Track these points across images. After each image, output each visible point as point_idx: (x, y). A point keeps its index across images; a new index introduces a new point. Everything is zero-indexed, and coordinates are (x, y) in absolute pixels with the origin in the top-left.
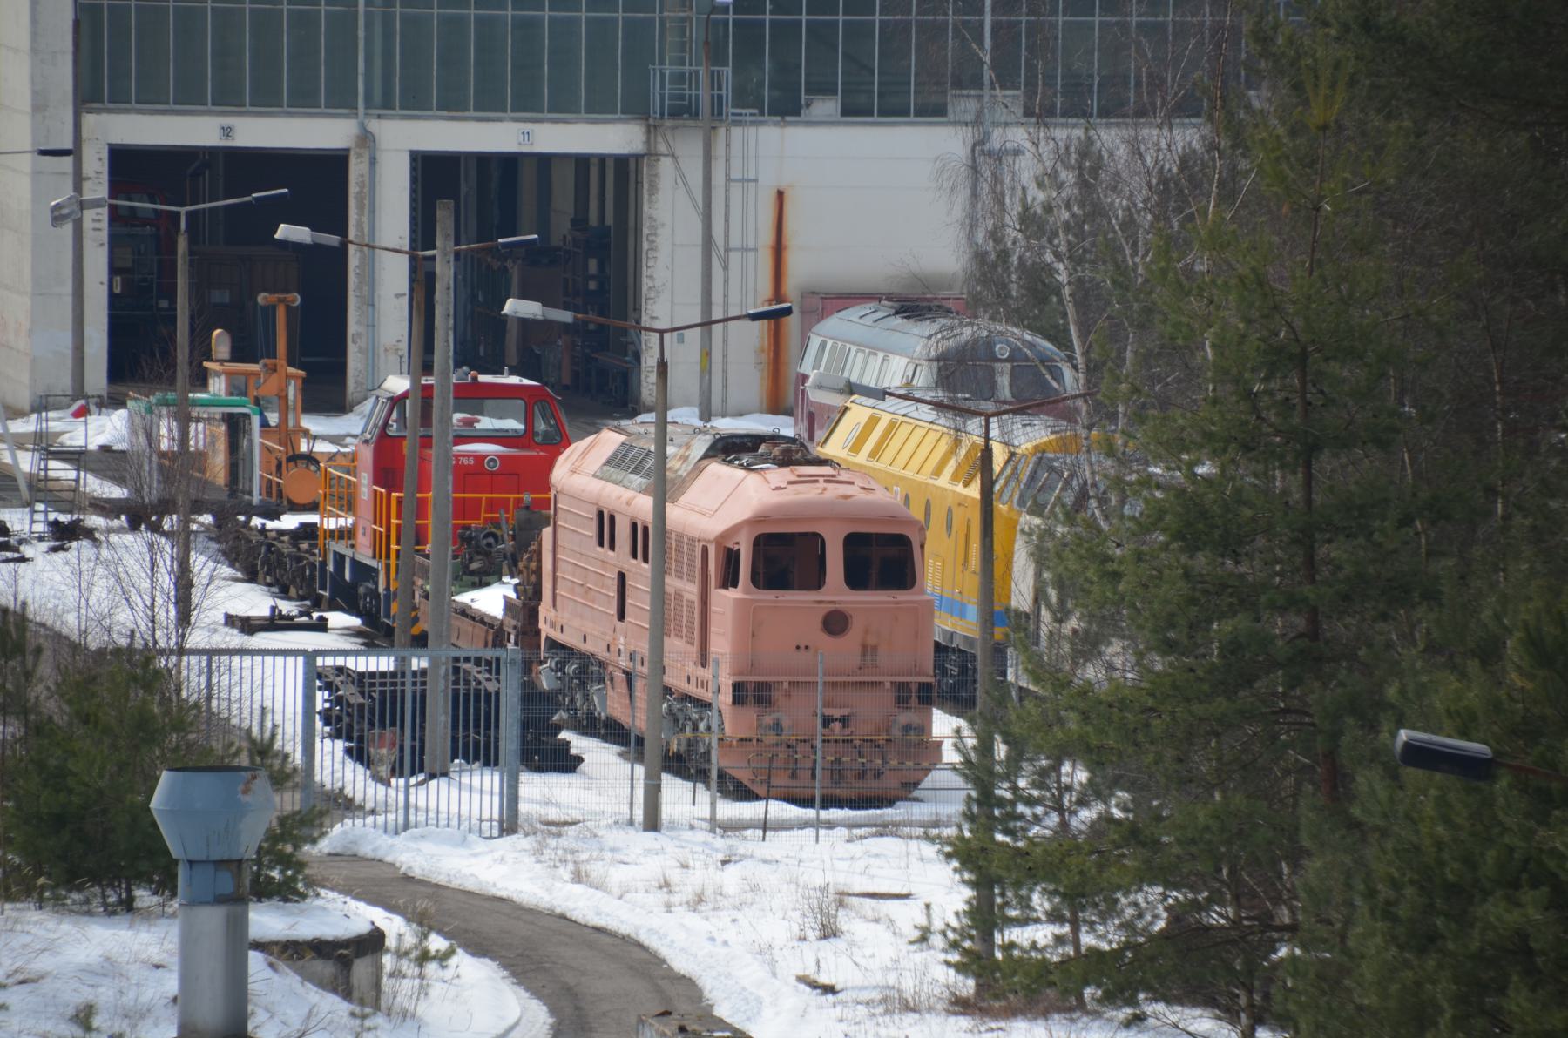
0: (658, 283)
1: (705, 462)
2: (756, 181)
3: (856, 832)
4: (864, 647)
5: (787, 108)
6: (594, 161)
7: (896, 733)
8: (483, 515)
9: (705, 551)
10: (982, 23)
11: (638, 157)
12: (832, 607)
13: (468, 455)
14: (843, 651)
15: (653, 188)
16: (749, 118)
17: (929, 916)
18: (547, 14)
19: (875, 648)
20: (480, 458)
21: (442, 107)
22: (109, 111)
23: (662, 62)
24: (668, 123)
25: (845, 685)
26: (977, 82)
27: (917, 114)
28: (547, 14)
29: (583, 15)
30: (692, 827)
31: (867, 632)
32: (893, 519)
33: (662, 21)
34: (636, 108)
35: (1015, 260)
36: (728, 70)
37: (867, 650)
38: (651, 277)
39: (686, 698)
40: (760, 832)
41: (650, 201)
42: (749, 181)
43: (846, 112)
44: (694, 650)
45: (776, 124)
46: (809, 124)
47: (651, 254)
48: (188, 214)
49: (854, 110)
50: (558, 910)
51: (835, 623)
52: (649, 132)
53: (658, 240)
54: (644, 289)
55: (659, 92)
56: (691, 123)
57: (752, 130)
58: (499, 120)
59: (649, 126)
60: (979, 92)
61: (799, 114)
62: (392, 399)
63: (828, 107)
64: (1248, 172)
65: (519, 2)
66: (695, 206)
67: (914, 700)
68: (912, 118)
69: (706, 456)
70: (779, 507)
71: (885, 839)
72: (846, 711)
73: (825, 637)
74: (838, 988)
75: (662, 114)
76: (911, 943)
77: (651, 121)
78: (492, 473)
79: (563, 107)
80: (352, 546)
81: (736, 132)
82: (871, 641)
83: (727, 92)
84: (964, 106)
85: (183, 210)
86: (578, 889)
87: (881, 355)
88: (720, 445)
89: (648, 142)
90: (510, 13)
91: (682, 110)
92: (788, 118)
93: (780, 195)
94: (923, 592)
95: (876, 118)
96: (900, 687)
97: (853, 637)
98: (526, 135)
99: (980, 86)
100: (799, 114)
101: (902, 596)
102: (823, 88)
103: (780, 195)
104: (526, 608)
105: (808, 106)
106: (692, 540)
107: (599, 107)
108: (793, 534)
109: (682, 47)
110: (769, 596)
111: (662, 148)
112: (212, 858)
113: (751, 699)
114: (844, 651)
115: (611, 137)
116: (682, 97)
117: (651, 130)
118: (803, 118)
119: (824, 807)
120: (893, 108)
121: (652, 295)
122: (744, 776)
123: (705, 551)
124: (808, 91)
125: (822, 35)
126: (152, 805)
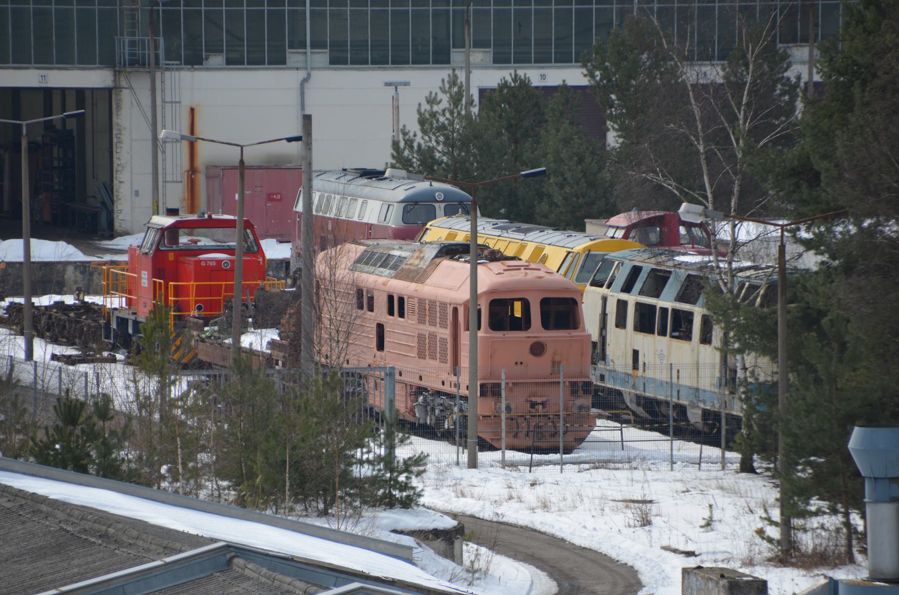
0: (123, 162)
1: (438, 260)
2: (179, 102)
3: (582, 466)
4: (554, 363)
5: (195, 60)
6: (88, 94)
7: (575, 410)
8: (223, 294)
9: (455, 310)
10: (305, 10)
11: (109, 90)
12: (536, 340)
13: (212, 260)
14: (540, 366)
15: (119, 107)
16: (175, 67)
17: (711, 512)
18: (53, 7)
19: (559, 363)
20: (219, 262)
21: (81, 62)
22: (373, 69)
23: (122, 34)
24: (129, 70)
25: (543, 384)
26: (304, 46)
27: (269, 63)
28: (53, 7)
29: (492, 8)
30: (492, 466)
31: (555, 353)
32: (567, 290)
33: (121, 11)
34: (108, 61)
35: (415, 145)
36: (161, 40)
37: (555, 364)
38: (119, 159)
39: (439, 393)
40: (528, 468)
41: (117, 115)
42: (176, 102)
43: (332, 62)
44: (449, 365)
45: (189, 70)
46: (208, 69)
47: (119, 145)
48: (27, 125)
49: (233, 62)
50: (468, 513)
51: (537, 349)
52: (115, 75)
53: (123, 137)
54: (115, 165)
55: (124, 50)
56: (142, 69)
57: (177, 73)
58: (27, 68)
59: (115, 71)
60: (303, 50)
61: (202, 64)
62: (162, 229)
63: (217, 60)
64: (781, 95)
65: (659, 2)
66: (145, 116)
67: (581, 392)
68: (349, 66)
69: (436, 257)
70: (503, 284)
71: (600, 470)
72: (544, 399)
73: (532, 357)
74: (697, 553)
75: (125, 64)
76: (702, 527)
77: (117, 69)
78: (226, 270)
79: (65, 61)
80: (134, 314)
81: (167, 74)
82: (557, 358)
83: (161, 52)
84: (293, 57)
85: (24, 123)
86: (462, 500)
87: (360, 201)
88: (444, 250)
89: (115, 81)
90: (31, 6)
91: (137, 63)
92: (195, 66)
93: (192, 110)
94: (584, 330)
95: (246, 66)
96: (573, 384)
97: (547, 357)
98: (43, 77)
99: (305, 47)
100: (202, 64)
101: (574, 333)
102: (215, 49)
103: (192, 110)
104: (294, 346)
105: (207, 59)
106: (444, 305)
107: (86, 61)
108: (506, 300)
109: (133, 26)
110: (499, 334)
111: (124, 83)
112: (889, 476)
113: (489, 393)
114: (542, 365)
115: (94, 78)
116: (134, 55)
117: (117, 74)
118: (204, 66)
119: (565, 453)
120: (256, 61)
121: (120, 169)
122: (487, 437)
123: (455, 310)
124: (206, 51)
125: (213, 20)
126: (851, 445)
